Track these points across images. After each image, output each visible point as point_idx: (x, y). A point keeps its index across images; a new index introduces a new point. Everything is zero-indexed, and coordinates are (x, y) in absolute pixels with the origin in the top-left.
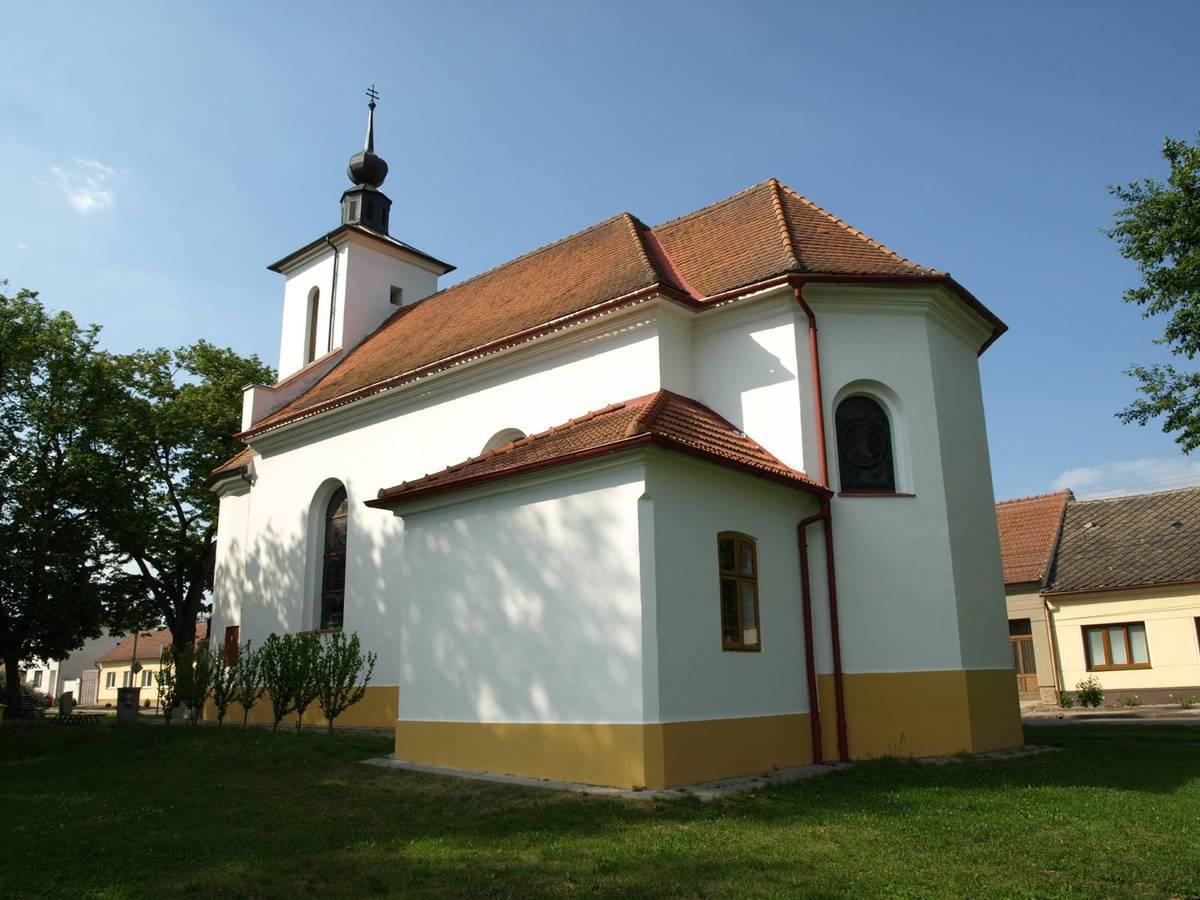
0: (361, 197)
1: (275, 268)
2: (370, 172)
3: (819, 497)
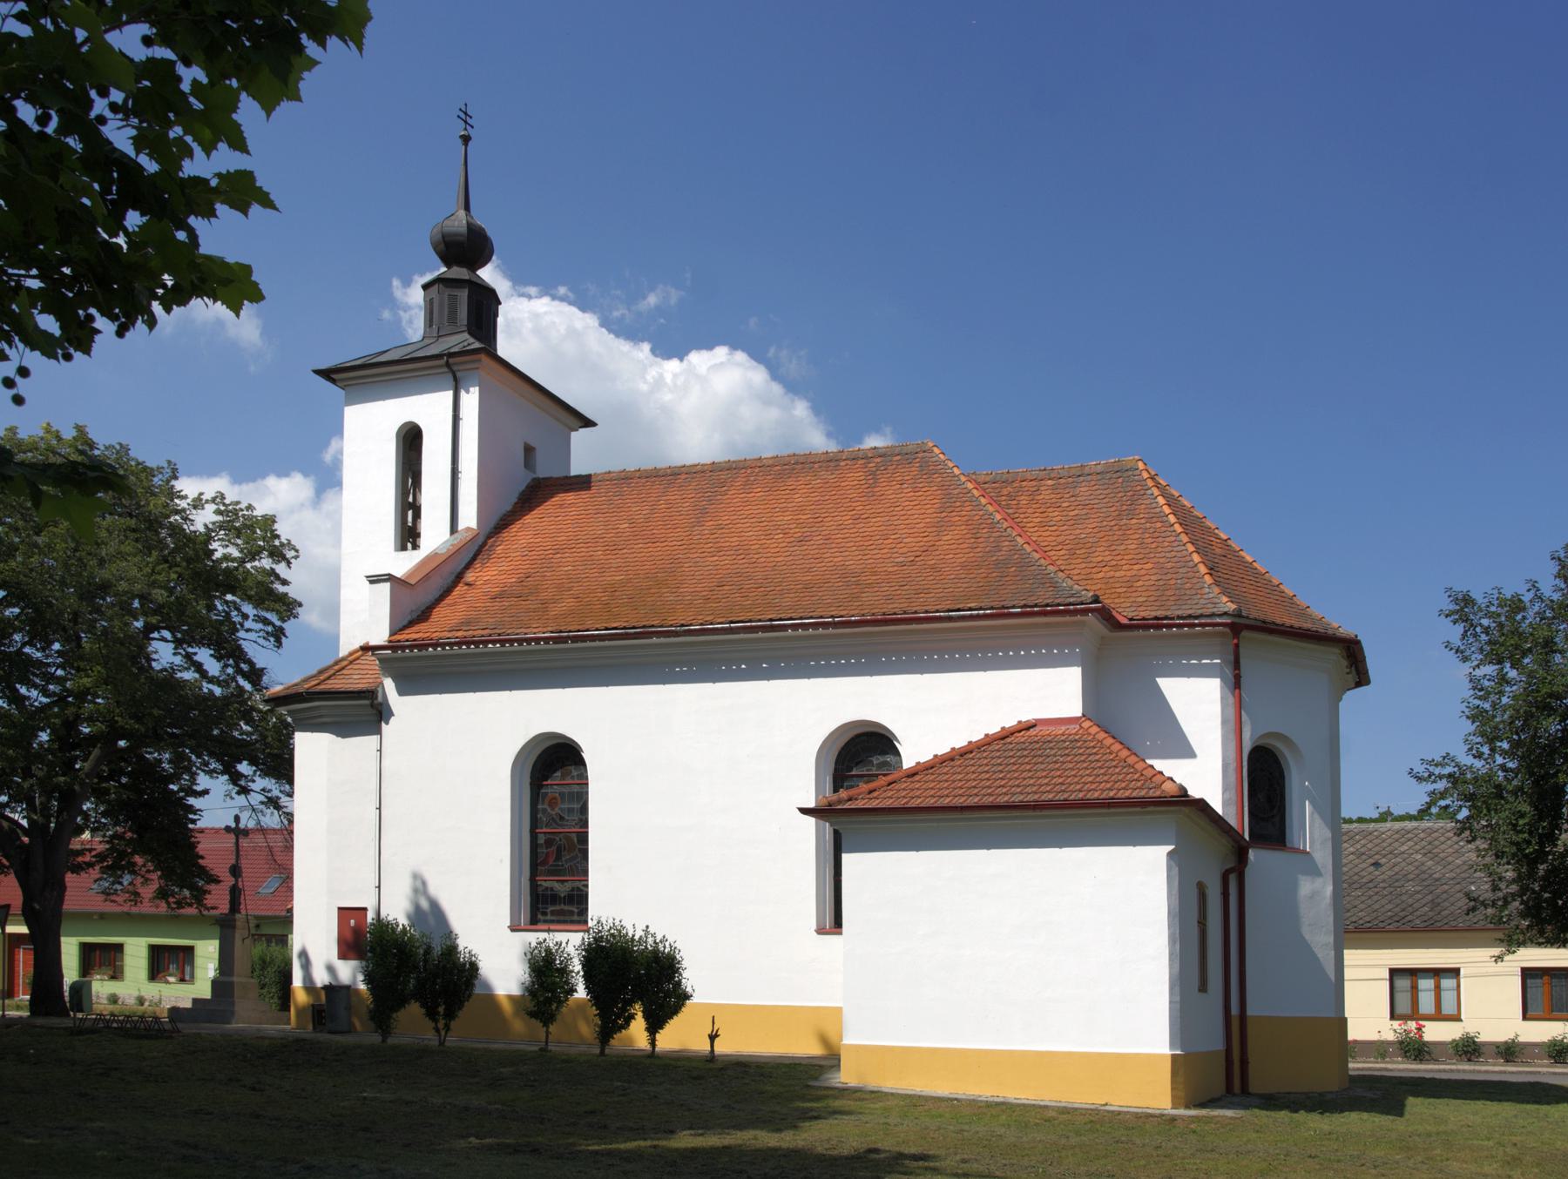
1: (327, 374)
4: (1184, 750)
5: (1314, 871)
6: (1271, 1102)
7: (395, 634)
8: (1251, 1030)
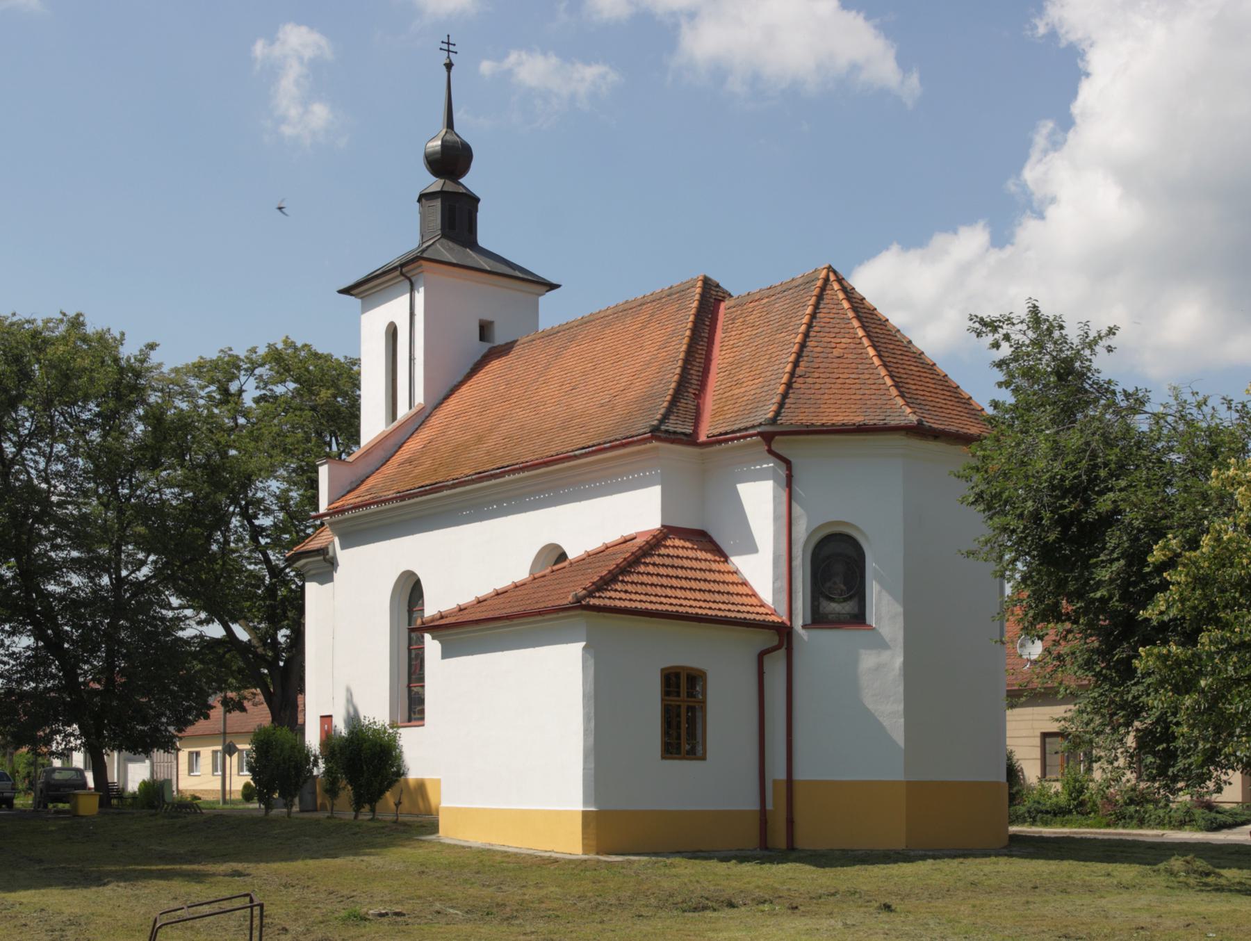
0: (439, 200)
3: (784, 632)
5: (882, 645)
6: (821, 859)
7: (333, 503)
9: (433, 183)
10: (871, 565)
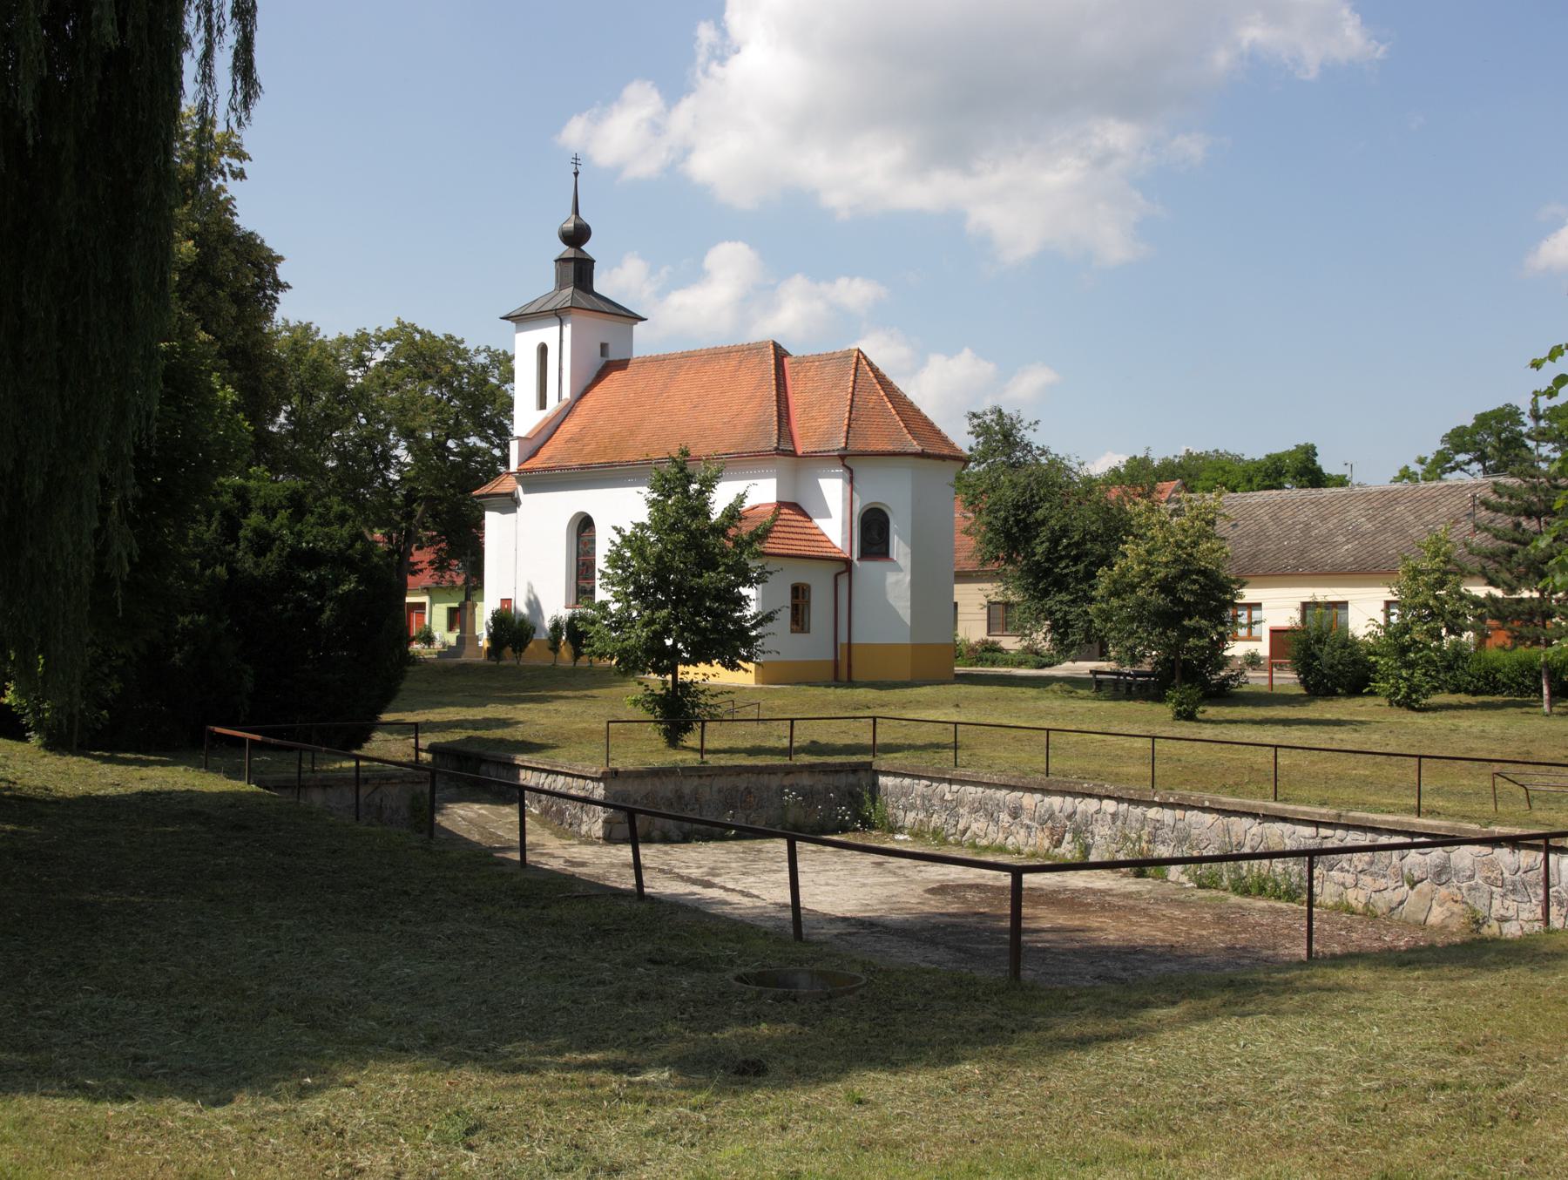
2: (577, 236)
3: (848, 562)
4: (826, 514)
5: (899, 569)
8: (854, 650)
9: (562, 249)
10: (893, 526)
